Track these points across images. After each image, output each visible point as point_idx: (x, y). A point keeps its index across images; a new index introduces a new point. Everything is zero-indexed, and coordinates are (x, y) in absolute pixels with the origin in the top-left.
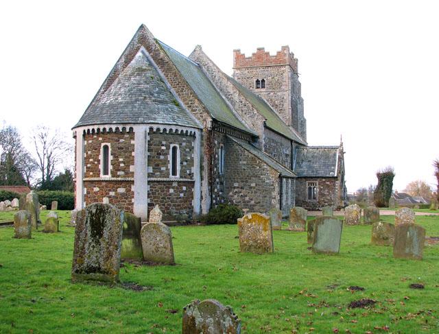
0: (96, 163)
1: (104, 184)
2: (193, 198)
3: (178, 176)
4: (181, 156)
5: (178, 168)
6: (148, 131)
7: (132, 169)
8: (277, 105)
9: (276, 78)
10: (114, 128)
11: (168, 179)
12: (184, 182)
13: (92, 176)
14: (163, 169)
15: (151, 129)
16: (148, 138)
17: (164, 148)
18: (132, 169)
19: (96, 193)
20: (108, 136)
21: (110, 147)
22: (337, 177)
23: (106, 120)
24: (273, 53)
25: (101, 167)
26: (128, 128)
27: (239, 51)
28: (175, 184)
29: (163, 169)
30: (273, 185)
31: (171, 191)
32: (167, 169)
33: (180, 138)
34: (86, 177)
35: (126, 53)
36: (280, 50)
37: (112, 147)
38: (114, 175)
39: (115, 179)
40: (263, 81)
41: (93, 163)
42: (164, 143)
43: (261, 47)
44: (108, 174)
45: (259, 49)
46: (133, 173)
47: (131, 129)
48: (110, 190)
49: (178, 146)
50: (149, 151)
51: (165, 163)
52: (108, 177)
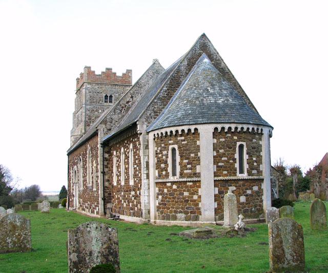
0: (231, 161)
1: (241, 183)
10: (251, 127)
13: (226, 175)
20: (243, 135)
21: (177, 149)
23: (242, 120)
24: (119, 74)
25: (237, 165)
27: (90, 68)
30: (275, 182)
34: (218, 176)
35: (189, 56)
36: (125, 72)
37: (247, 146)
38: (249, 173)
39: (250, 177)
40: (111, 97)
41: (227, 162)
43: (109, 67)
44: (176, 175)
45: (107, 69)
46: (199, 173)
47: (196, 129)
48: (247, 189)
52: (245, 176)
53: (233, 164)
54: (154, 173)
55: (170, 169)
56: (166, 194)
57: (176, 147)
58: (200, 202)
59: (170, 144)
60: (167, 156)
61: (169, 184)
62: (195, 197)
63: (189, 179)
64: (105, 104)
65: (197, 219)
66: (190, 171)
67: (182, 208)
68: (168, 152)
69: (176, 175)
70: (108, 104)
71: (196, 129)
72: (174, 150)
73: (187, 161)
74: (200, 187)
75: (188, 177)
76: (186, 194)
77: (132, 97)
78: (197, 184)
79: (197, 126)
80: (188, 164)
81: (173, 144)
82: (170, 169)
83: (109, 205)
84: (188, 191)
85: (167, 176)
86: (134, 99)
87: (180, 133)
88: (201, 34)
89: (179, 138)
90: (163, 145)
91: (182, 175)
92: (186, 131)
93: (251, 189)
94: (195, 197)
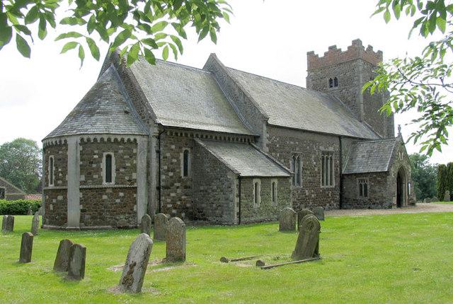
2: (135, 203)
3: (113, 182)
4: (116, 163)
5: (114, 175)
6: (79, 141)
8: (349, 102)
9: (348, 74)
11: (101, 186)
12: (120, 188)
14: (96, 176)
15: (82, 139)
16: (80, 148)
17: (96, 157)
22: (388, 172)
26: (63, 140)
27: (313, 52)
28: (108, 191)
29: (96, 176)
31: (105, 197)
32: (100, 177)
33: (115, 146)
40: (336, 79)
42: (96, 152)
47: (65, 141)
49: (112, 154)
50: (81, 160)
51: (98, 170)
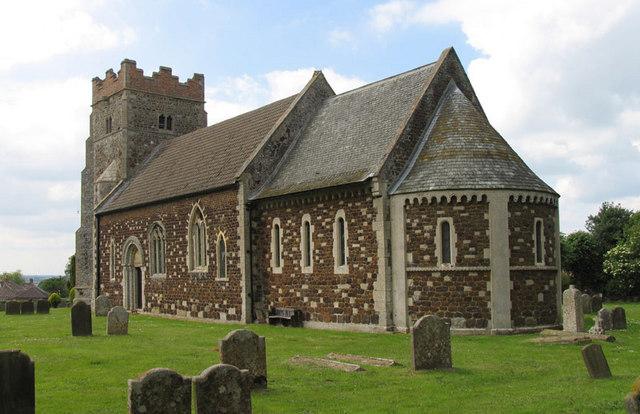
0: (529, 244)
7: (487, 254)
13: (522, 264)
18: (487, 254)
19: (530, 287)
27: (134, 63)
38: (547, 264)
40: (170, 119)
44: (449, 262)
45: (162, 69)
47: (484, 197)
53: (530, 249)
54: (400, 256)
55: (438, 253)
56: (431, 289)
57: (450, 220)
58: (489, 300)
59: (439, 216)
60: (433, 233)
61: (437, 275)
62: (482, 294)
63: (471, 268)
64: (160, 131)
65: (484, 324)
66: (473, 256)
67: (462, 310)
68: (434, 228)
69: (449, 262)
70: (165, 131)
71: (484, 197)
72: (445, 225)
73: (469, 242)
74: (489, 280)
75: (470, 265)
76: (467, 288)
77: (288, 131)
78: (485, 276)
79: (487, 193)
80: (471, 245)
81: (443, 216)
82: (438, 253)
83: (257, 305)
84: (471, 285)
85: (433, 261)
86: (292, 134)
87: (459, 200)
88: (449, 47)
89: (455, 208)
90: (424, 216)
91: (459, 261)
92: (439, 200)
93: (310, 300)
94: (482, 294)
